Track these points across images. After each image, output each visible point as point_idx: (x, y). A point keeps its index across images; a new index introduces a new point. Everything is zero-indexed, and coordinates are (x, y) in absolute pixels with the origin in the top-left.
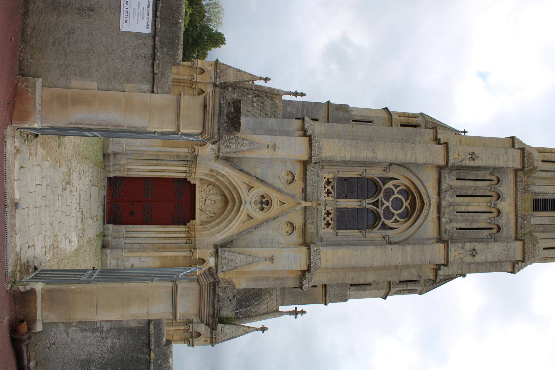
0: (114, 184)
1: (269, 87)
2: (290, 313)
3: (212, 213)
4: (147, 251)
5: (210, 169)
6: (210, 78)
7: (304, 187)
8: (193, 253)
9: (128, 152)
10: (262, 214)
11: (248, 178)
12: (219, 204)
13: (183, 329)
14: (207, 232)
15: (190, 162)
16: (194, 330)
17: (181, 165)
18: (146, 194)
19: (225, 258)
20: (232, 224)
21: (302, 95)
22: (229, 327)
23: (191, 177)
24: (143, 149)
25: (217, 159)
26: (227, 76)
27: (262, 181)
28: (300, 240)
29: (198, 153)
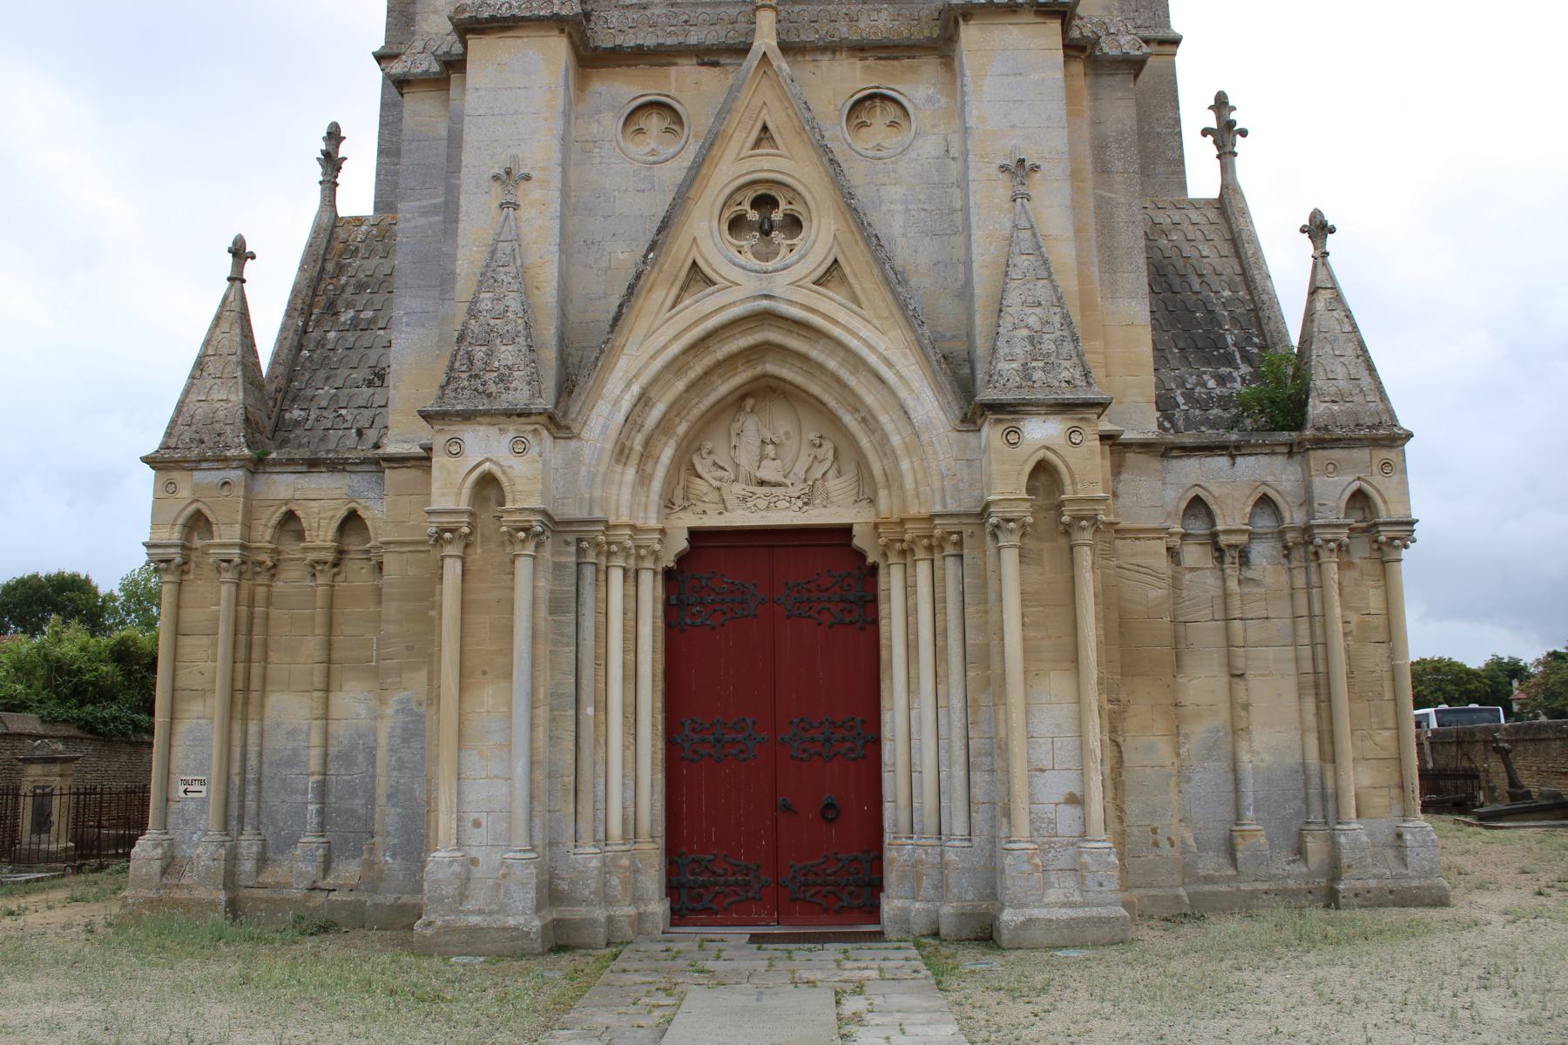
0: (700, 896)
1: (297, 265)
2: (1226, 154)
3: (820, 453)
4: (1002, 734)
5: (618, 461)
6: (226, 487)
7: (694, 61)
8: (1009, 520)
9: (539, 839)
10: (815, 222)
11: (650, 289)
12: (780, 422)
13: (1335, 566)
14: (905, 465)
15: (584, 550)
16: (1342, 521)
17: (602, 595)
18: (742, 752)
19: (1026, 372)
20: (865, 352)
21: (334, 136)
22: (1320, 370)
23: (657, 547)
24: (520, 768)
25: (568, 428)
26: (221, 414)
27: (665, 226)
28: (929, 67)
29: (533, 511)
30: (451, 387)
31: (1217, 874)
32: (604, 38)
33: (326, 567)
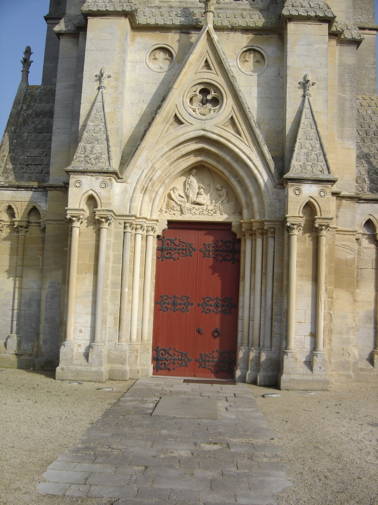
5: (141, 192)
7: (179, 31)
21: (28, 52)
30: (77, 160)
31: (366, 368)
32: (141, 20)
33: (23, 229)
